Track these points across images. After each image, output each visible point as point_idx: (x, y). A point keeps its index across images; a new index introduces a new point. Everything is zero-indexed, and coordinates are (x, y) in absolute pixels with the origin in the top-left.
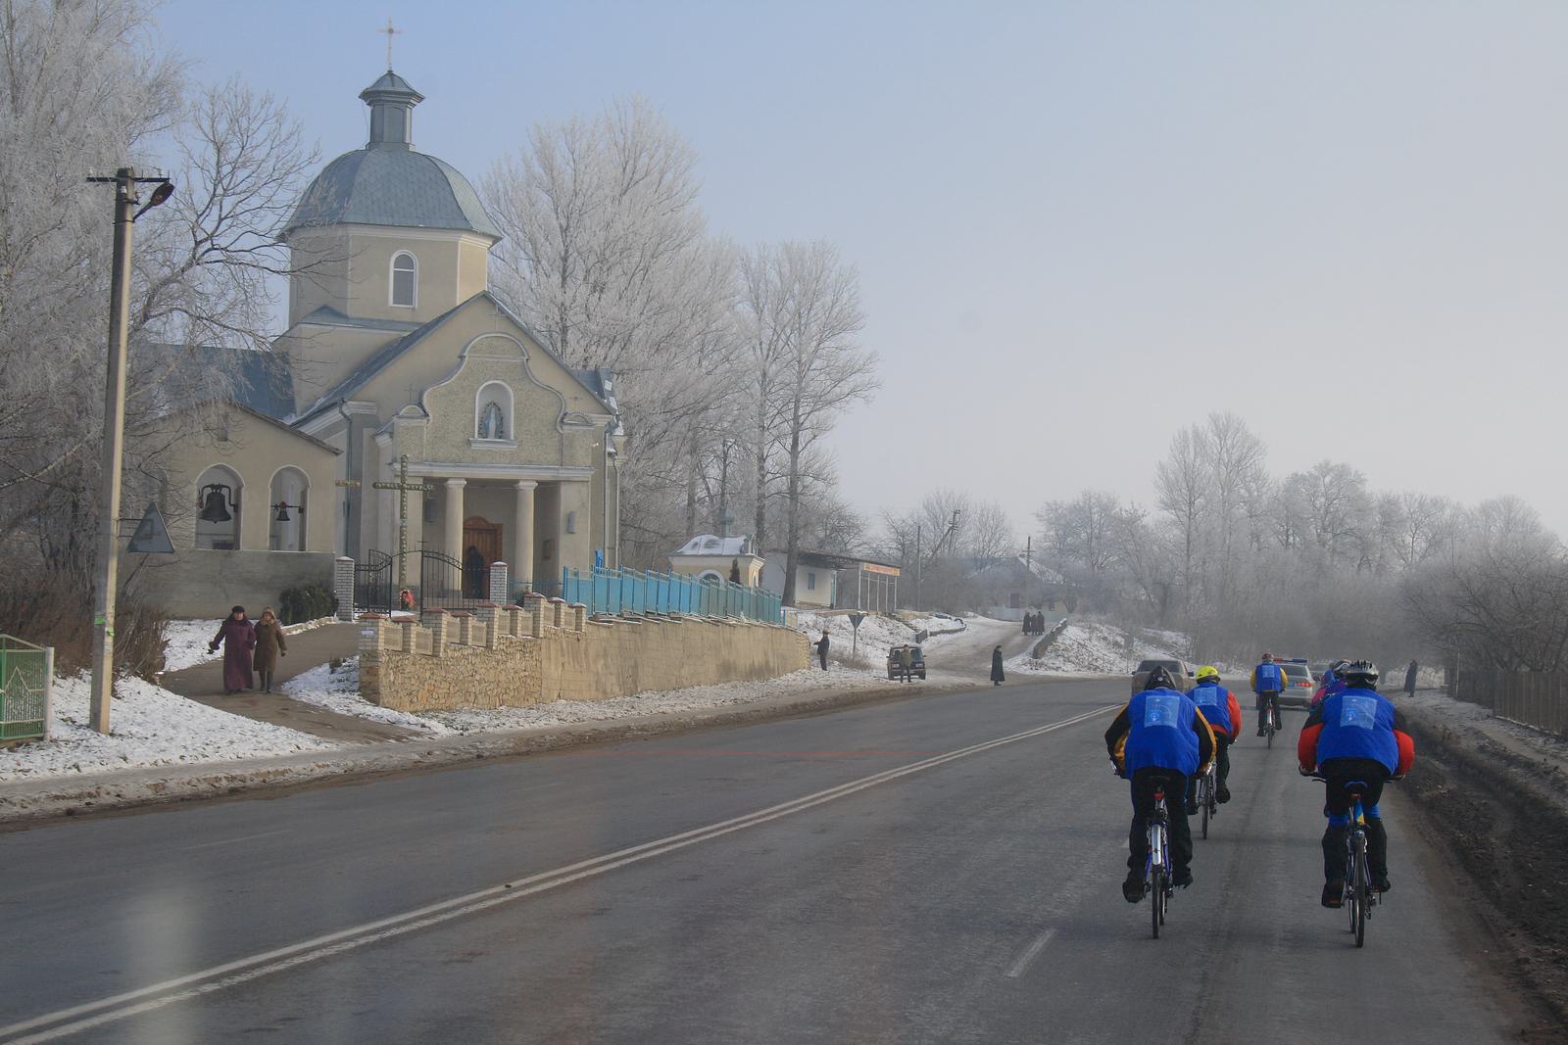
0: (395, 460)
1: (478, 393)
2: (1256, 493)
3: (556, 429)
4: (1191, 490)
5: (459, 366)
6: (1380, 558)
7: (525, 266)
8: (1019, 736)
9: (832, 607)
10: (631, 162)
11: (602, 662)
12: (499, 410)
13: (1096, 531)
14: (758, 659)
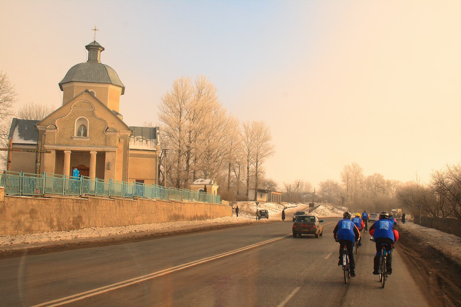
1: (76, 121)
3: (104, 133)
9: (266, 201)
10: (201, 90)
12: (85, 127)
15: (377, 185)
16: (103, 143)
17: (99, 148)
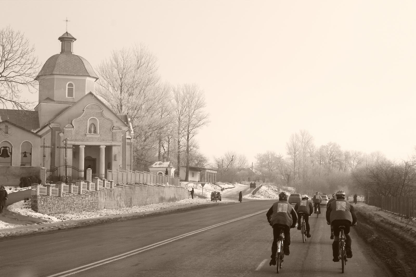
0: (64, 140)
1: (89, 120)
2: (312, 150)
3: (111, 131)
4: (295, 149)
5: (83, 112)
6: (345, 167)
7: (111, 88)
8: (239, 219)
9: (199, 182)
11: (119, 197)
12: (95, 125)
13: (270, 161)
14: (172, 196)
15: (332, 158)
16: (110, 138)
17: (108, 143)
